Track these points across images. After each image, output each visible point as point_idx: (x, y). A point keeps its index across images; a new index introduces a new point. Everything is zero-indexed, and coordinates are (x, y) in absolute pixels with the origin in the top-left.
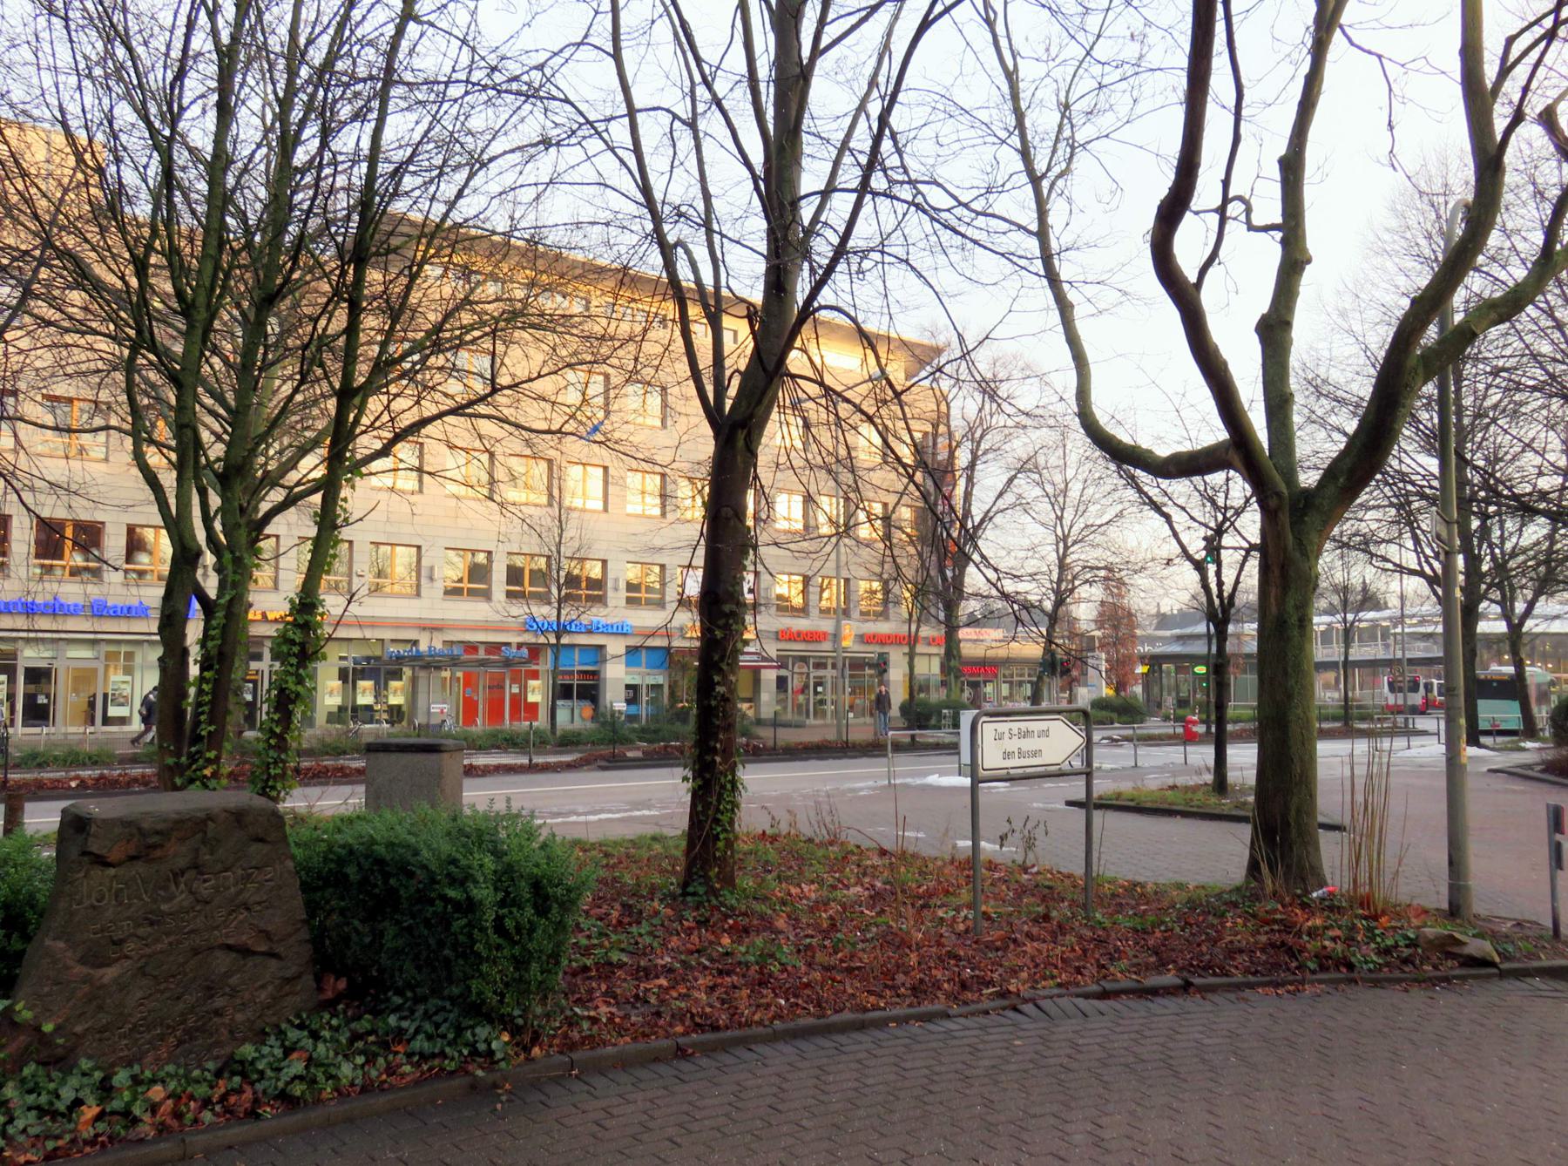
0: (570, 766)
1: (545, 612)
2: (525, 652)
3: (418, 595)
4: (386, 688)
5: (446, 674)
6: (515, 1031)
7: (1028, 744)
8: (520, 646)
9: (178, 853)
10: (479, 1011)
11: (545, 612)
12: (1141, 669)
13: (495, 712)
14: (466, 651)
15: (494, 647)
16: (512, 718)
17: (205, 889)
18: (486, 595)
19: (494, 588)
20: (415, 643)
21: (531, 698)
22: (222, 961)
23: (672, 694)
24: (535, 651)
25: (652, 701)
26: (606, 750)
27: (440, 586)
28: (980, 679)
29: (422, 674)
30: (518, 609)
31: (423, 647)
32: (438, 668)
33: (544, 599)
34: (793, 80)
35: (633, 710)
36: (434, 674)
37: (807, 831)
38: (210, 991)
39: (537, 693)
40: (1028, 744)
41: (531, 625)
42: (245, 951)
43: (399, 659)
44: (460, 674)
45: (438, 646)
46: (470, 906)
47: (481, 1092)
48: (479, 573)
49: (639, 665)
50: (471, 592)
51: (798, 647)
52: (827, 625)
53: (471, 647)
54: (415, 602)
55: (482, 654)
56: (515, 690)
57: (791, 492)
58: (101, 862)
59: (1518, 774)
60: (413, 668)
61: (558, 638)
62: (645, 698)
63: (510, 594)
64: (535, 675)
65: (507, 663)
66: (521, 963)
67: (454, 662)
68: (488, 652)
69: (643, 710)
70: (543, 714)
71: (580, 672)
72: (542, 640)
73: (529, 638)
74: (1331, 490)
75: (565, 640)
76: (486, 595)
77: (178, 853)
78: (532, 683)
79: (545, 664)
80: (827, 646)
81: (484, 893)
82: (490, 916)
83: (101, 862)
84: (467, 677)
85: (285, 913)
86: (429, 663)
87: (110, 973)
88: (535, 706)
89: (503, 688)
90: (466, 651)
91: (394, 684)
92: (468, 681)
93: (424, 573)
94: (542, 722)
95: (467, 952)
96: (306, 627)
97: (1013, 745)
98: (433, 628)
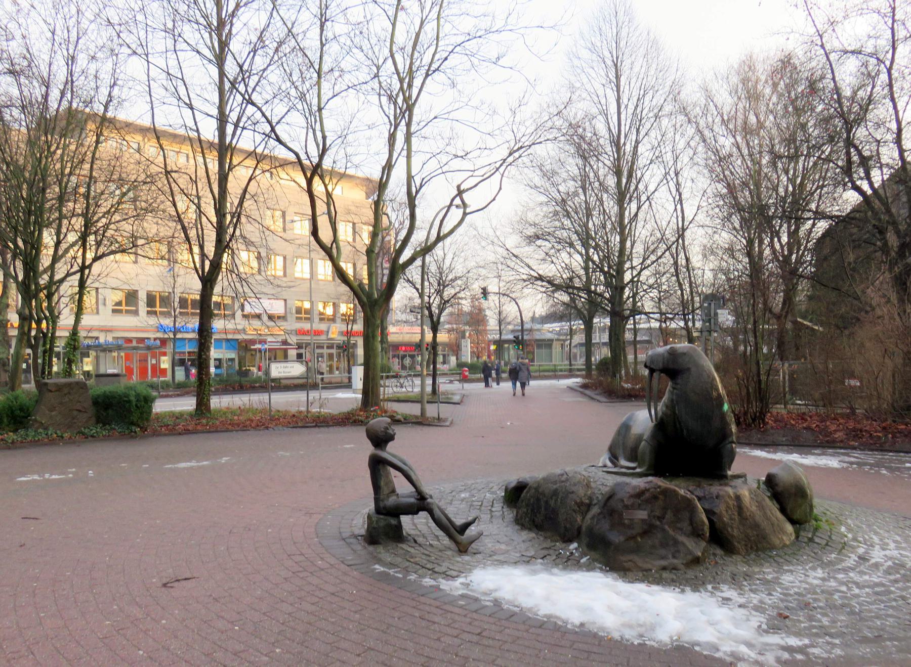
0: (178, 395)
1: (167, 322)
2: (158, 342)
3: (98, 313)
4: (82, 362)
5: (115, 354)
6: (141, 428)
7: (286, 370)
8: (155, 339)
9: (66, 391)
10: (132, 423)
11: (167, 322)
12: (493, 347)
13: (143, 371)
14: (126, 342)
15: (141, 340)
16: (152, 377)
17: (71, 398)
18: (136, 313)
19: (140, 308)
20: (97, 338)
21: (163, 366)
22: (75, 413)
23: (240, 363)
24: (164, 342)
25: (229, 367)
26: (767, 648)
27: (110, 306)
28: (416, 353)
29: (102, 354)
30: (153, 321)
31: (102, 340)
32: (110, 351)
33: (166, 314)
34: (223, 179)
35: (219, 371)
36: (108, 354)
37: (255, 406)
38: (74, 418)
39: (165, 363)
40: (286, 370)
41: (161, 328)
42: (80, 411)
43: (89, 347)
44: (123, 354)
45: (110, 339)
46: (129, 402)
47: (132, 437)
48: (131, 297)
49: (221, 348)
50: (127, 312)
51: (307, 338)
52: (323, 327)
53: (129, 340)
54: (96, 317)
55: (134, 344)
56: (154, 362)
57: (302, 258)
58: (51, 391)
59: (571, 389)
60: (96, 351)
61: (175, 335)
62: (225, 365)
63: (148, 312)
64: (165, 354)
65: (148, 348)
66: (141, 414)
67: (119, 348)
68: (138, 342)
69: (223, 371)
70: (169, 373)
71: (189, 353)
72: (166, 336)
73: (160, 335)
74: (381, 300)
75: (179, 336)
76: (136, 313)
77: (66, 391)
78: (163, 358)
79: (169, 349)
80: (323, 337)
81: (133, 398)
82: (134, 404)
83: (51, 391)
84: (127, 355)
85: (88, 404)
86: (105, 349)
87: (53, 413)
88: (882, 624)
89: (147, 361)
90: (126, 342)
91: (86, 360)
92: (128, 358)
93: (100, 302)
94: (169, 377)
95: (129, 411)
96: (75, 340)
97: (282, 370)
98: (107, 330)
